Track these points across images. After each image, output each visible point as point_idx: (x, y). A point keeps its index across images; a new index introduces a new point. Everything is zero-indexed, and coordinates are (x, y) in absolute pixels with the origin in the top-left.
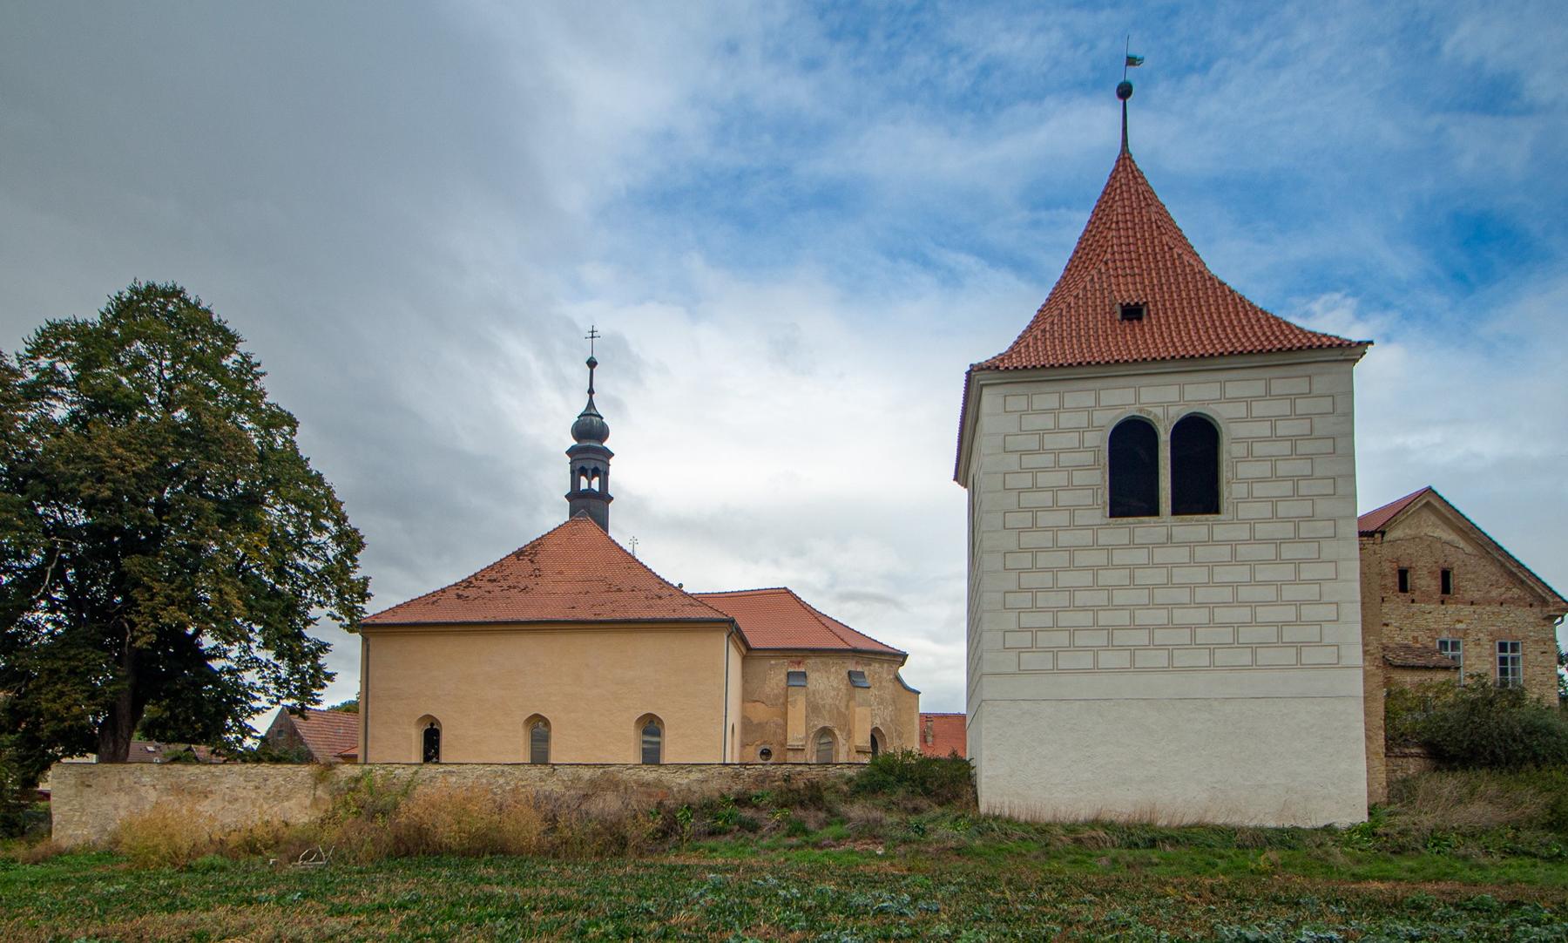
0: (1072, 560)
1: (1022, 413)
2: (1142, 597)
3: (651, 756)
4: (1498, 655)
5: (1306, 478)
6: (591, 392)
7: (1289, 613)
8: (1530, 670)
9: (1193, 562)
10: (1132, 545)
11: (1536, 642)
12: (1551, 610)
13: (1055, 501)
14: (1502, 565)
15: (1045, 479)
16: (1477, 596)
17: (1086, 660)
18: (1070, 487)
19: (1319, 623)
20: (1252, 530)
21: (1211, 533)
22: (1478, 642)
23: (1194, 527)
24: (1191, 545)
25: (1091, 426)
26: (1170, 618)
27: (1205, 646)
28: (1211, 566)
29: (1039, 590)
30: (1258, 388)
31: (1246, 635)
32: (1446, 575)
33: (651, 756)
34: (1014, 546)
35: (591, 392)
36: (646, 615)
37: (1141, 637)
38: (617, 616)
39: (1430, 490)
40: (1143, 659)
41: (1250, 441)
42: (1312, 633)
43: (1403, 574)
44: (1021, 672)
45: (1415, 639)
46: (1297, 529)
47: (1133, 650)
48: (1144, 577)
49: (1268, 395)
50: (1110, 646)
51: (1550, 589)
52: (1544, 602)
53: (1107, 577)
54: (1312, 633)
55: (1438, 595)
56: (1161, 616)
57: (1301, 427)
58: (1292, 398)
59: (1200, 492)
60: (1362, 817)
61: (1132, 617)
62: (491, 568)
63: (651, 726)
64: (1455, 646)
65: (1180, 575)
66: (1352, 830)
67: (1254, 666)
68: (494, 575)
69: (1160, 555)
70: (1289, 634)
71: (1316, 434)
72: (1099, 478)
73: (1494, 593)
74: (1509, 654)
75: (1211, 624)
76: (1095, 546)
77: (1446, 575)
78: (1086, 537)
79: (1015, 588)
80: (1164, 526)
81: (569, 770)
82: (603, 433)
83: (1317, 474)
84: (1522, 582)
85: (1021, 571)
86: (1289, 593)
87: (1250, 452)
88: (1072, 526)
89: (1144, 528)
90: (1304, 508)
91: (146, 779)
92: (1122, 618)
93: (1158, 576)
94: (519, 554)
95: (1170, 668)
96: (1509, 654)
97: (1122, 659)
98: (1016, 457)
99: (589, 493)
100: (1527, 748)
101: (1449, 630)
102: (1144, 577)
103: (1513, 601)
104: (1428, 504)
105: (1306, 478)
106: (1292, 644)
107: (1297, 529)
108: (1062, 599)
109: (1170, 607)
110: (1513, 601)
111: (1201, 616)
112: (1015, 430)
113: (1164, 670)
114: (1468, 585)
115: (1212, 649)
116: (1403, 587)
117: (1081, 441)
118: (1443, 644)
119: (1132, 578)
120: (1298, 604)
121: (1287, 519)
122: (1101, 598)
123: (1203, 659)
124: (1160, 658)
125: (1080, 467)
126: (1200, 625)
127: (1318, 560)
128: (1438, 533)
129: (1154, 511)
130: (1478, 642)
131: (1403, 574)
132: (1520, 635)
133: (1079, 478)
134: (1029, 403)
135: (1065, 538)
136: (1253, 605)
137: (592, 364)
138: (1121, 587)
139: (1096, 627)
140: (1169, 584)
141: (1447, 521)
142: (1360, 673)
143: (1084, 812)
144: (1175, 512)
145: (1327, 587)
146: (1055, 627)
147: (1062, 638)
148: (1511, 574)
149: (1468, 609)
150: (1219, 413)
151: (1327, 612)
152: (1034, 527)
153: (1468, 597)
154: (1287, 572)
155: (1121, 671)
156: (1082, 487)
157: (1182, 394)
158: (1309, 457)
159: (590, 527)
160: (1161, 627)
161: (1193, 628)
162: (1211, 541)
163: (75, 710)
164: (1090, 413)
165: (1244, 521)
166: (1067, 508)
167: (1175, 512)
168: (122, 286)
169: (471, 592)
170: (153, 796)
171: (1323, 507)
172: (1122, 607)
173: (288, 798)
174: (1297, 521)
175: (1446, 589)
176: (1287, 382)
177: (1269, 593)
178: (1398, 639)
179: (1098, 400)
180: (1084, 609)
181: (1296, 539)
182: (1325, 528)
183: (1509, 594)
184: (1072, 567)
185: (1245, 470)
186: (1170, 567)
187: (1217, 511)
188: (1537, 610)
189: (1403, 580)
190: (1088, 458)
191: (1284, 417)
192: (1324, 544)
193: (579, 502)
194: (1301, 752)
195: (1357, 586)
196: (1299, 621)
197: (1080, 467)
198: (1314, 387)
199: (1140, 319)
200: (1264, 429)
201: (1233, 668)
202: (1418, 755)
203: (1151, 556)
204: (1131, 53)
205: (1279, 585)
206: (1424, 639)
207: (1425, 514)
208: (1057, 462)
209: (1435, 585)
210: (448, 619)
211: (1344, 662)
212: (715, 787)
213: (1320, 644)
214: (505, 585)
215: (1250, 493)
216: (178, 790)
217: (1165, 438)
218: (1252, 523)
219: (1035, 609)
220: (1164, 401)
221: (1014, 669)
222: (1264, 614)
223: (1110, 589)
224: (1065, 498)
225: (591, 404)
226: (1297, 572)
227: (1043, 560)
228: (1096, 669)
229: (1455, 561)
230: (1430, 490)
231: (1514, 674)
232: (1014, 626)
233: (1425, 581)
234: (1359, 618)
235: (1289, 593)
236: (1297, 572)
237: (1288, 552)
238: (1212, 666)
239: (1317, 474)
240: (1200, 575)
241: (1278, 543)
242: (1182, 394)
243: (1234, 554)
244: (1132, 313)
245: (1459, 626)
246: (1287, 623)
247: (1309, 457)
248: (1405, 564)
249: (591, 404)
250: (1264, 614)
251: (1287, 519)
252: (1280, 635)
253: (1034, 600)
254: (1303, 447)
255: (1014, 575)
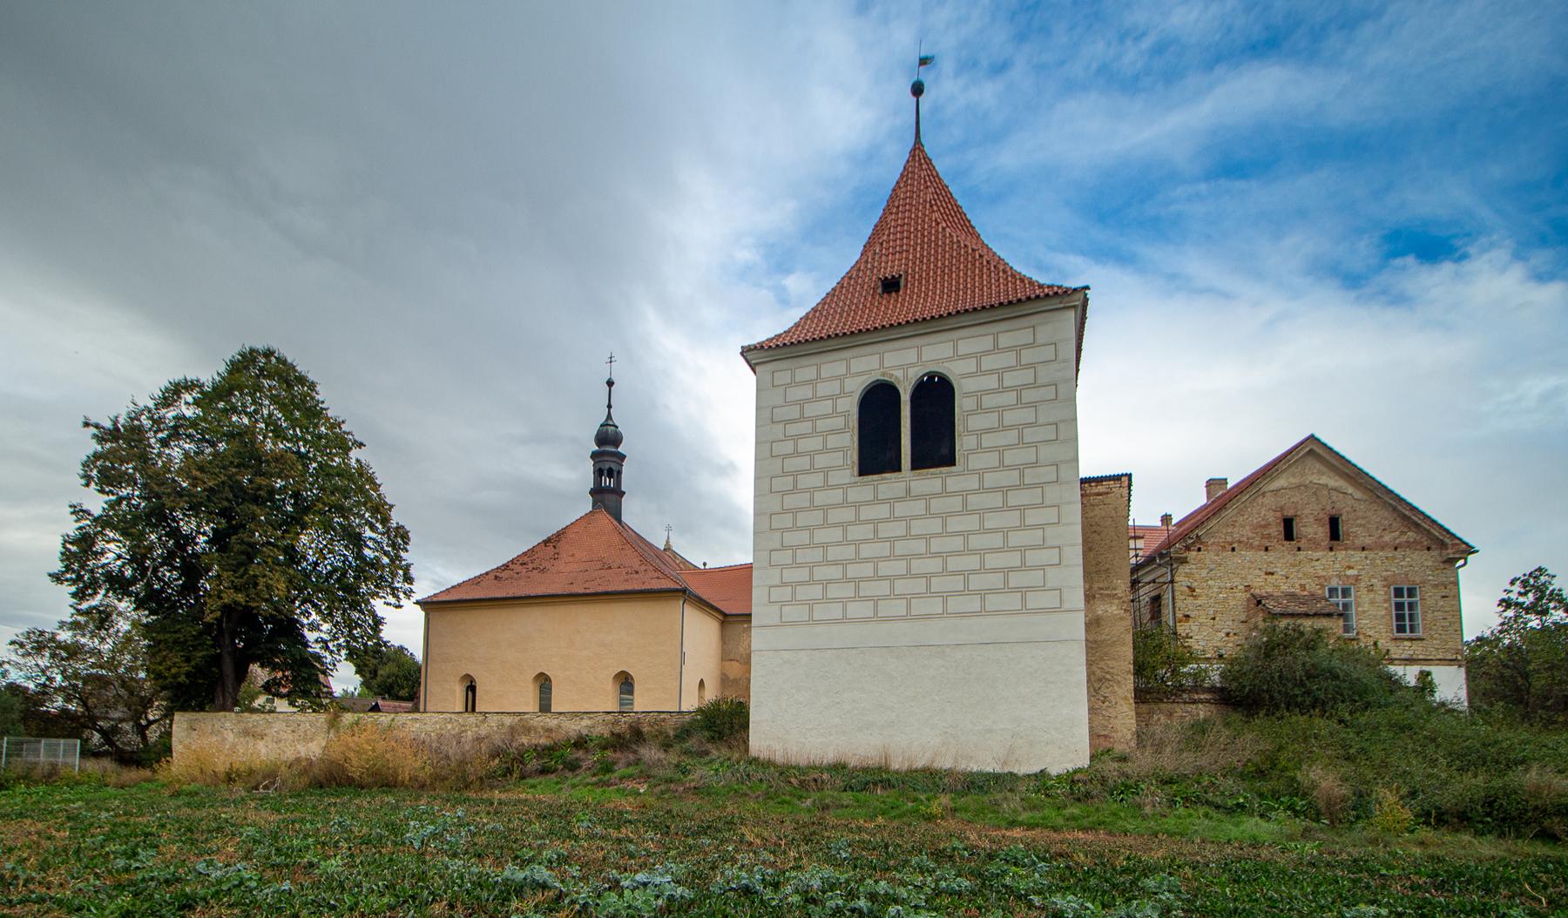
0: (825, 518)
1: (787, 386)
2: (885, 549)
3: (545, 707)
4: (1394, 600)
5: (1030, 425)
6: (609, 406)
7: (1014, 559)
8: (1430, 615)
9: (929, 514)
10: (876, 501)
11: (1436, 586)
12: (1450, 553)
13: (812, 464)
14: (1395, 509)
15: (804, 445)
16: (1368, 541)
17: (836, 611)
18: (825, 450)
19: (1042, 568)
20: (981, 480)
21: (944, 484)
22: (1371, 588)
23: (930, 481)
24: (927, 497)
25: (843, 393)
26: (909, 569)
27: (938, 594)
28: (944, 516)
29: (798, 547)
30: (986, 343)
31: (976, 582)
32: (1334, 523)
33: (545, 707)
34: (777, 508)
35: (609, 406)
36: (622, 588)
37: (882, 588)
38: (600, 589)
39: (1312, 438)
40: (886, 608)
41: (979, 395)
42: (1035, 578)
43: (1288, 524)
44: (783, 624)
45: (1303, 587)
46: (1022, 475)
47: (876, 600)
48: (887, 530)
49: (996, 349)
50: (858, 597)
51: (1448, 531)
52: (1443, 545)
53: (856, 532)
54: (1035, 578)
55: (1326, 542)
56: (899, 567)
57: (1026, 376)
58: (1017, 349)
59: (937, 449)
60: (1084, 761)
61: (876, 570)
62: (525, 554)
63: (544, 684)
64: (1346, 592)
65: (918, 527)
66: (1071, 779)
67: (983, 612)
68: (526, 559)
69: (901, 509)
70: (1016, 580)
71: (1040, 382)
72: (848, 441)
73: (1387, 538)
74: (1406, 600)
75: (945, 572)
76: (845, 503)
77: (1334, 523)
78: (836, 496)
79: (778, 546)
80: (907, 481)
81: (496, 717)
82: (616, 440)
83: (1041, 420)
84: (1417, 525)
85: (784, 530)
86: (1016, 539)
87: (979, 406)
88: (827, 486)
89: (888, 484)
90: (1028, 455)
91: (228, 724)
92: (867, 570)
93: (898, 529)
94: (546, 542)
95: (908, 617)
96: (1406, 600)
97: (865, 609)
98: (781, 426)
99: (608, 490)
100: (1308, 693)
101: (1339, 576)
102: (887, 530)
103: (1409, 545)
104: (1311, 452)
105: (1030, 425)
106: (1017, 590)
107: (1022, 475)
108: (817, 555)
109: (908, 557)
110: (1409, 545)
111: (934, 565)
112: (781, 402)
113: (940, 616)
114: (1359, 530)
115: (945, 596)
116: (1289, 535)
117: (835, 407)
118: (1333, 591)
119: (876, 532)
120: (1022, 550)
121: (1012, 468)
122: (848, 552)
123: (974, 604)
124: (899, 607)
125: (834, 432)
126: (934, 575)
127: (1042, 505)
128: (1324, 480)
129: (896, 467)
130: (1371, 588)
131: (1288, 524)
132: (1418, 580)
133: (833, 441)
134: (793, 376)
135: (820, 498)
136: (981, 552)
137: (610, 383)
138: (866, 541)
139: (846, 580)
140: (908, 536)
141: (1333, 469)
142: (1082, 614)
143: (830, 757)
144: (914, 468)
145: (1049, 531)
146: (811, 582)
147: (816, 591)
148: (1405, 517)
149: (1358, 556)
150: (954, 371)
151: (1050, 556)
152: (795, 489)
153: (1358, 542)
154: (1013, 518)
155: (866, 620)
156: (835, 450)
157: (919, 355)
158: (1034, 405)
159: (604, 519)
160: (902, 577)
161: (928, 577)
162: (944, 493)
163: (174, 671)
164: (846, 377)
165: (973, 472)
166: (821, 470)
167: (914, 468)
168: (232, 352)
169: (504, 575)
170: (231, 737)
171: (1046, 453)
172: (867, 560)
173: (312, 740)
174: (1021, 469)
175: (1335, 535)
176: (1012, 335)
177: (996, 540)
178: (1284, 587)
179: (848, 368)
180: (835, 563)
181: (1022, 486)
182: (1048, 474)
183: (1404, 538)
184: (826, 525)
185: (975, 422)
186: (908, 519)
187: (951, 461)
188: (1435, 553)
189: (1288, 529)
190: (839, 422)
191: (1010, 369)
192: (1048, 488)
193: (599, 497)
194: (1023, 699)
195: (1079, 528)
196: (1024, 567)
197: (834, 432)
198: (1038, 336)
199: (898, 291)
200: (991, 382)
201: (963, 615)
202: (1208, 701)
203: (892, 511)
204: (923, 54)
205: (1005, 532)
206: (1312, 587)
207: (1310, 462)
208: (814, 428)
209: (1323, 532)
210: (482, 596)
211: (1066, 606)
212: (603, 730)
213: (1043, 588)
214: (530, 566)
215: (979, 444)
216: (246, 733)
217: (905, 398)
218: (981, 473)
219: (795, 565)
220: (903, 365)
221: (776, 621)
222: (992, 561)
223: (857, 543)
224: (821, 461)
225: (609, 417)
226: (1023, 518)
227: (802, 519)
228: (844, 620)
229: (1344, 507)
230: (1312, 438)
231: (1411, 619)
232: (777, 582)
233: (1312, 529)
234: (1081, 561)
235: (1016, 539)
236: (1023, 518)
237: (1015, 498)
238: (945, 614)
239: (1041, 420)
240: (934, 526)
241: (1005, 490)
242: (919, 355)
243: (965, 503)
244: (891, 285)
245: (1350, 572)
246: (1012, 569)
247: (1034, 405)
248: (1290, 513)
249: (609, 417)
250: (992, 561)
251: (1012, 468)
252: (1006, 582)
253: (794, 556)
254: (1029, 396)
255: (778, 534)
